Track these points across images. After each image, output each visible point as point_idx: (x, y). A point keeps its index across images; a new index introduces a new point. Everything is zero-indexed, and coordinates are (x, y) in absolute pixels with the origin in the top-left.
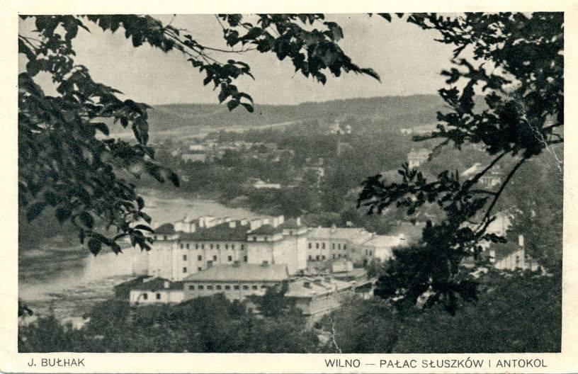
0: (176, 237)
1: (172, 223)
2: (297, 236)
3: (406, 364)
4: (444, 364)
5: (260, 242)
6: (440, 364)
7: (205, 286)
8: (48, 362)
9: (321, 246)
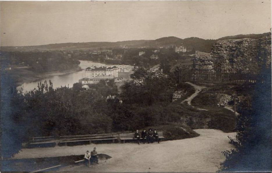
0: (91, 70)
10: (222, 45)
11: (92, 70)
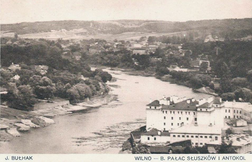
0: (160, 107)
1: (158, 100)
2: (220, 107)
3: (180, 158)
4: (198, 159)
5: (203, 111)
6: (196, 159)
7: (181, 135)
8: (15, 158)
9: (228, 111)
10: (215, 105)
11: (162, 109)
